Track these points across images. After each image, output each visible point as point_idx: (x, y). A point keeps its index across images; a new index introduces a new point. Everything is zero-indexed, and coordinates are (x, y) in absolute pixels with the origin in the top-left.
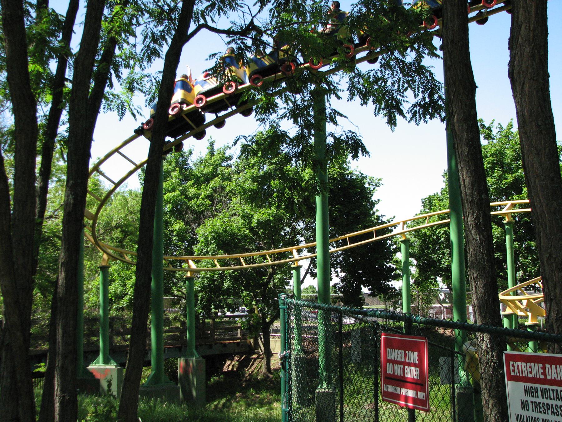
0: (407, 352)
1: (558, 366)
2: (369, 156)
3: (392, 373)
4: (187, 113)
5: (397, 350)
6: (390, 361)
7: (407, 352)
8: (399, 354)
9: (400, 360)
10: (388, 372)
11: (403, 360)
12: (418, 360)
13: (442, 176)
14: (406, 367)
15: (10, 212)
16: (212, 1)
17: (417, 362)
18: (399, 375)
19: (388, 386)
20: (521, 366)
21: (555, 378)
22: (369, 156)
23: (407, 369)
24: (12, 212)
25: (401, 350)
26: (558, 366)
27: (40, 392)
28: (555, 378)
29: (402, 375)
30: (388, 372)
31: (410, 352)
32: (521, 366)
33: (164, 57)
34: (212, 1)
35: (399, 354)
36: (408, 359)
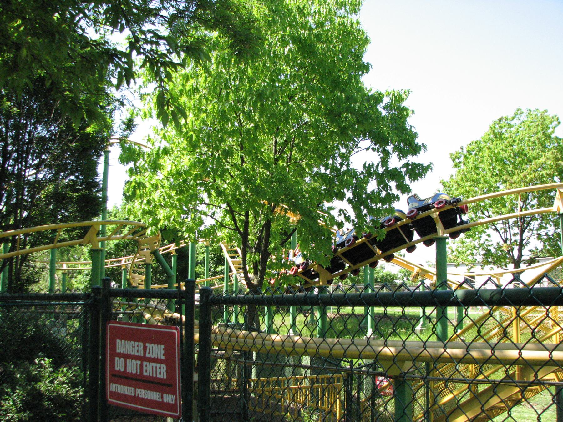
0: (147, 345)
1: (151, 375)
3: (122, 370)
4: (403, 246)
5: (132, 342)
6: (120, 355)
7: (147, 345)
9: (137, 354)
10: (117, 369)
11: (141, 354)
12: (164, 355)
13: (451, 155)
14: (145, 363)
17: (163, 358)
18: (134, 372)
19: (117, 385)
20: (156, 367)
23: (146, 366)
25: (139, 341)
26: (151, 375)
29: (138, 373)
30: (117, 369)
31: (152, 345)
32: (156, 367)
33: (117, 77)
36: (149, 353)
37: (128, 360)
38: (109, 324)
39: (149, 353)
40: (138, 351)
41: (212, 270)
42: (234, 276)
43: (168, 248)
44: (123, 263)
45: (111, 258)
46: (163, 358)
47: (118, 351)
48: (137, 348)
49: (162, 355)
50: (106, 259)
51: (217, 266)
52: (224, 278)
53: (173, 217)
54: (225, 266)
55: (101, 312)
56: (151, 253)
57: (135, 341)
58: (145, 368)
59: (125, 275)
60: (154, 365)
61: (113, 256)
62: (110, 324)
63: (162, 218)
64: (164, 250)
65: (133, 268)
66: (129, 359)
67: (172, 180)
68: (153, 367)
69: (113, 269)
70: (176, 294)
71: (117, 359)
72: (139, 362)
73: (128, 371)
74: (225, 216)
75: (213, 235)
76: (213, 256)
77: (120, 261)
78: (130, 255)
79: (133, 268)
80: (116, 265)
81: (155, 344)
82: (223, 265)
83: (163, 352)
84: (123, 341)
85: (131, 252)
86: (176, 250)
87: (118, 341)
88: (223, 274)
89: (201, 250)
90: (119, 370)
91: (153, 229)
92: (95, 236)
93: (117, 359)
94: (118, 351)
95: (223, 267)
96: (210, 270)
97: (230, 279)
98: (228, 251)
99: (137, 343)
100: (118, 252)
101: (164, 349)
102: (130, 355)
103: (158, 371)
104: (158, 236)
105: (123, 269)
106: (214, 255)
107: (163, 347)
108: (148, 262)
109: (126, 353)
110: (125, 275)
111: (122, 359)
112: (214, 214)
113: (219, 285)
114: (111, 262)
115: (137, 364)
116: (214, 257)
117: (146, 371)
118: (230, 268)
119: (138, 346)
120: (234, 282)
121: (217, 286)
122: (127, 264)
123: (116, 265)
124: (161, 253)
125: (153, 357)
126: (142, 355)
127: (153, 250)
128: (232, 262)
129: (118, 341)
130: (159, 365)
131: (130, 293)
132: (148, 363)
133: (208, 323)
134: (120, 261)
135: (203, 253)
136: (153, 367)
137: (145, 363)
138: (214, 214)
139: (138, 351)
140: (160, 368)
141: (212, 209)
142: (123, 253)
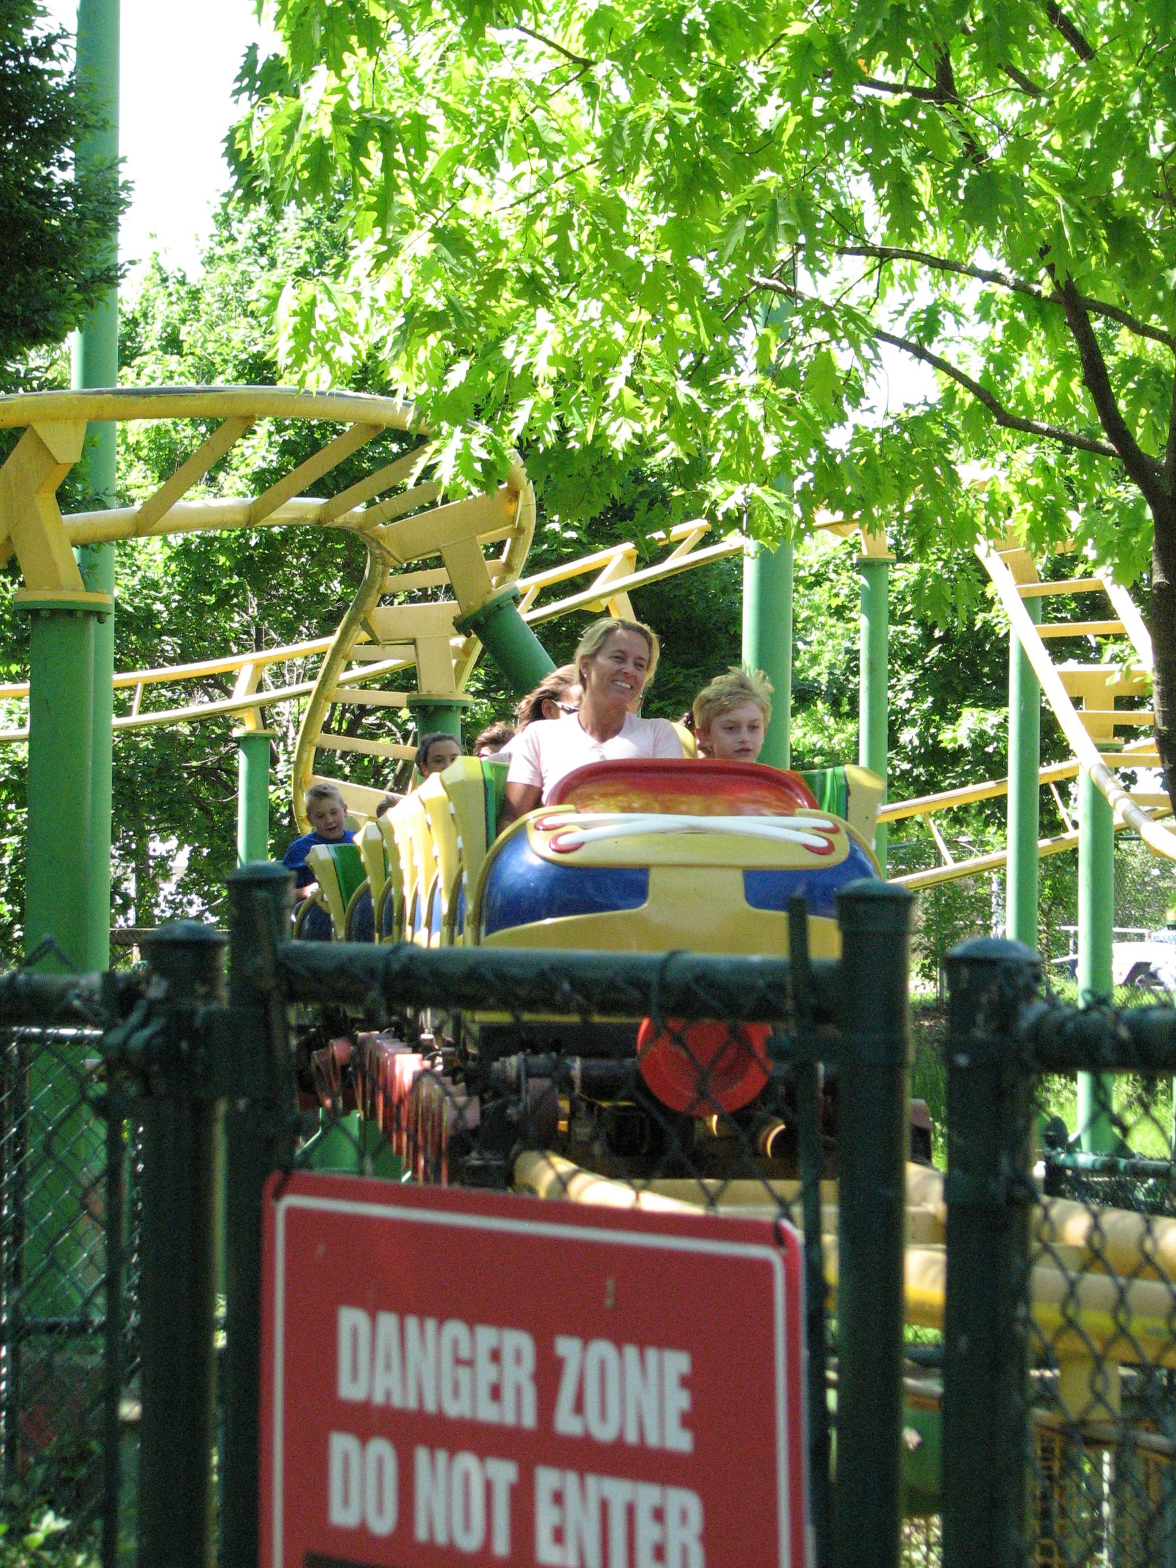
0: (567, 1347)
2: (253, 48)
3: (383, 1525)
5: (455, 1329)
7: (567, 1347)
8: (470, 1363)
9: (488, 1413)
10: (342, 1516)
12: (687, 1421)
14: (547, 1479)
15: (209, 1339)
16: (7, 801)
17: (680, 1441)
18: (470, 1542)
20: (631, 1511)
21: (388, 1395)
22: (253, 48)
23: (558, 1498)
24: (221, 1340)
25: (502, 1320)
27: (1125, 1382)
28: (388, 1395)
29: (501, 1546)
30: (342, 1516)
31: (602, 1349)
32: (631, 1511)
34: (7, 801)
35: (470, 1363)
36: (579, 1407)
37: (422, 1455)
38: (278, 1194)
39: (579, 1407)
40: (496, 1393)
41: (908, 736)
42: (1080, 791)
43: (588, 578)
44: (241, 694)
45: (151, 658)
46: (680, 1441)
47: (350, 1390)
48: (486, 1372)
49: (673, 1420)
50: (120, 667)
51: (945, 712)
52: (1000, 803)
53: (625, 368)
54: (1012, 710)
55: (222, 1108)
56: (462, 626)
57: (472, 1320)
58: (545, 1517)
59: (262, 778)
60: (618, 1490)
61: (169, 645)
62: (291, 1201)
63: (544, 370)
64: (548, 594)
65: (320, 738)
66: (432, 1447)
67: (621, 91)
68: (604, 1506)
69: (164, 737)
70: (776, 987)
71: (341, 1444)
72: (504, 1472)
73: (421, 1534)
74: (1017, 335)
75: (932, 486)
76: (913, 632)
77: (221, 683)
78: (289, 633)
79: (320, 738)
80: (200, 705)
81: (618, 1342)
82: (1000, 701)
83: (680, 1400)
84: (388, 1322)
85: (302, 611)
86: (636, 595)
87: (351, 1319)
88: (996, 767)
89: (821, 595)
90: (362, 1531)
91: (475, 441)
92: (47, 503)
93: (341, 1444)
94: (350, 1390)
95: (992, 717)
96: (893, 743)
97: (1047, 808)
98: (1028, 602)
99: (487, 1336)
100: (201, 609)
101: (686, 1382)
102: (440, 1419)
103: (647, 1533)
104: (514, 494)
105: (245, 741)
106: (927, 628)
107: (678, 1362)
108: (433, 685)
109: (412, 1404)
110: (262, 778)
111: (382, 1449)
112: (930, 324)
113: (961, 854)
114: (149, 688)
115: (489, 1487)
116: (928, 640)
117: (559, 1536)
118: (1050, 725)
119: (495, 1356)
120: (1081, 837)
121: (950, 866)
122: (273, 703)
123: (200, 705)
124: (526, 613)
125: (605, 1433)
126: (529, 1420)
127: (475, 605)
128: (1067, 680)
129: (351, 1319)
130: (648, 1495)
131: (436, 974)
132: (572, 1479)
133: (1012, 1201)
134: (221, 683)
135: (839, 612)
136: (604, 1506)
137: (547, 1479)
138: (930, 324)
139: (496, 1393)
140: (659, 1515)
141: (910, 281)
142: (237, 621)
